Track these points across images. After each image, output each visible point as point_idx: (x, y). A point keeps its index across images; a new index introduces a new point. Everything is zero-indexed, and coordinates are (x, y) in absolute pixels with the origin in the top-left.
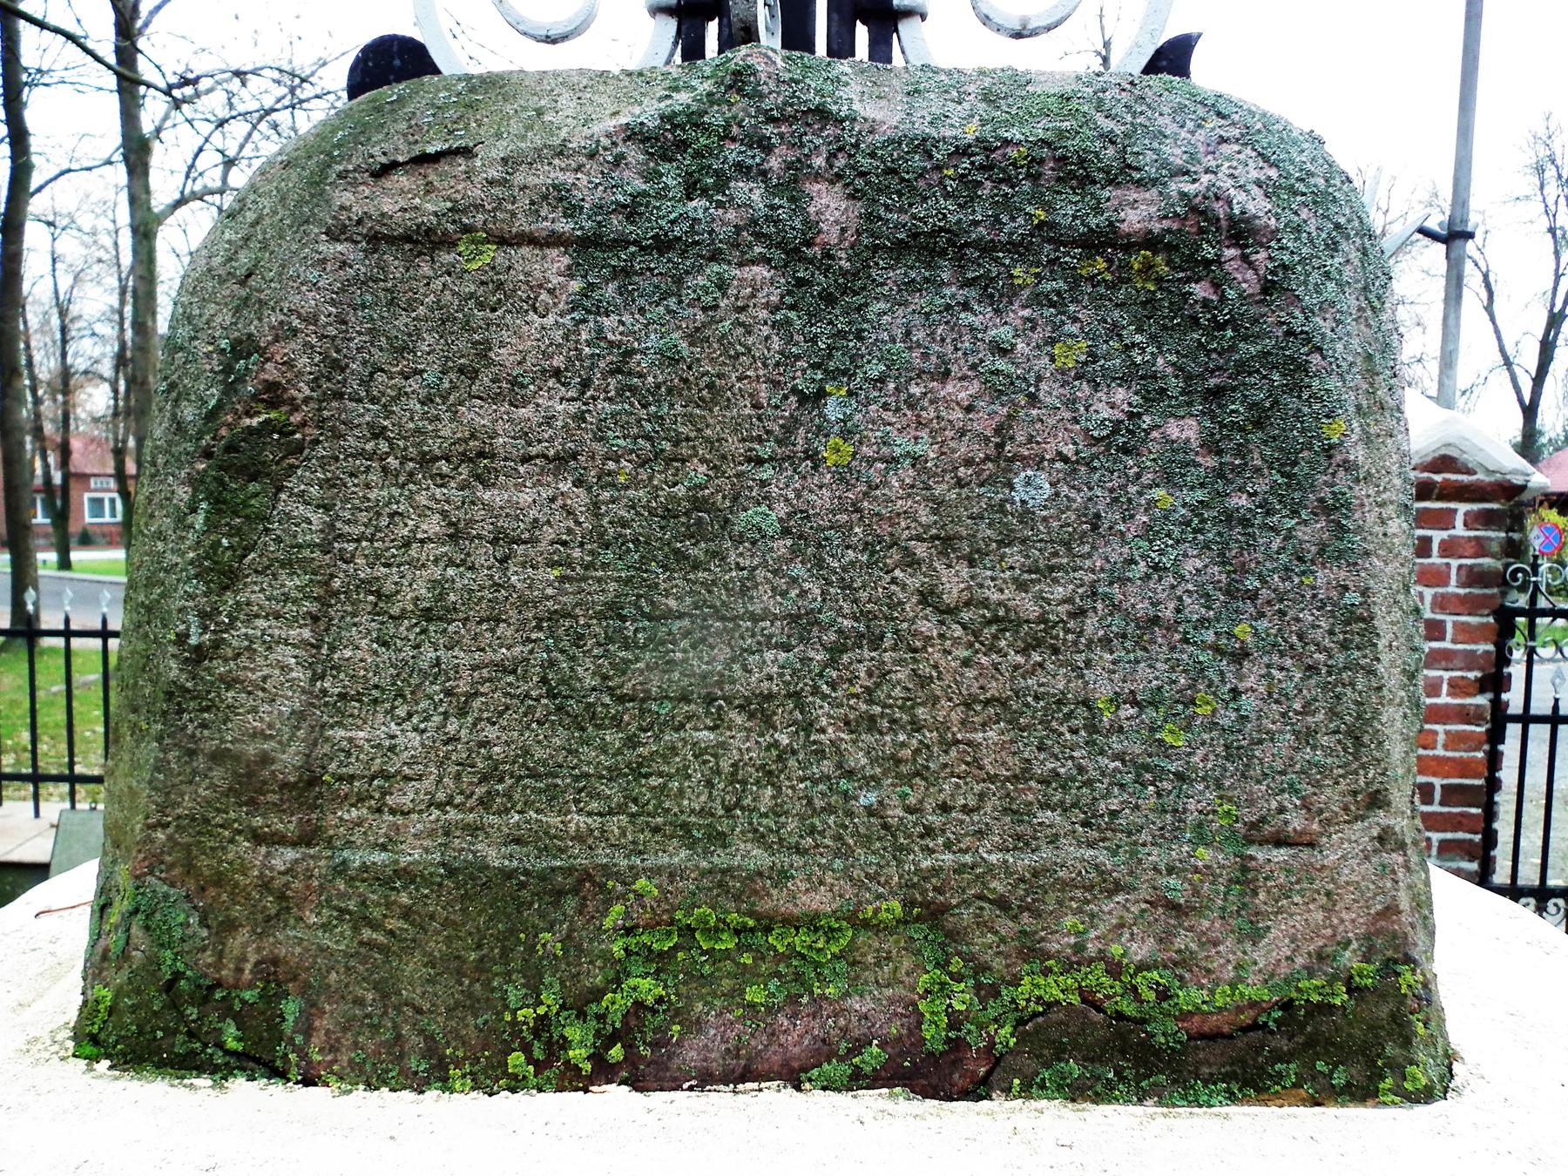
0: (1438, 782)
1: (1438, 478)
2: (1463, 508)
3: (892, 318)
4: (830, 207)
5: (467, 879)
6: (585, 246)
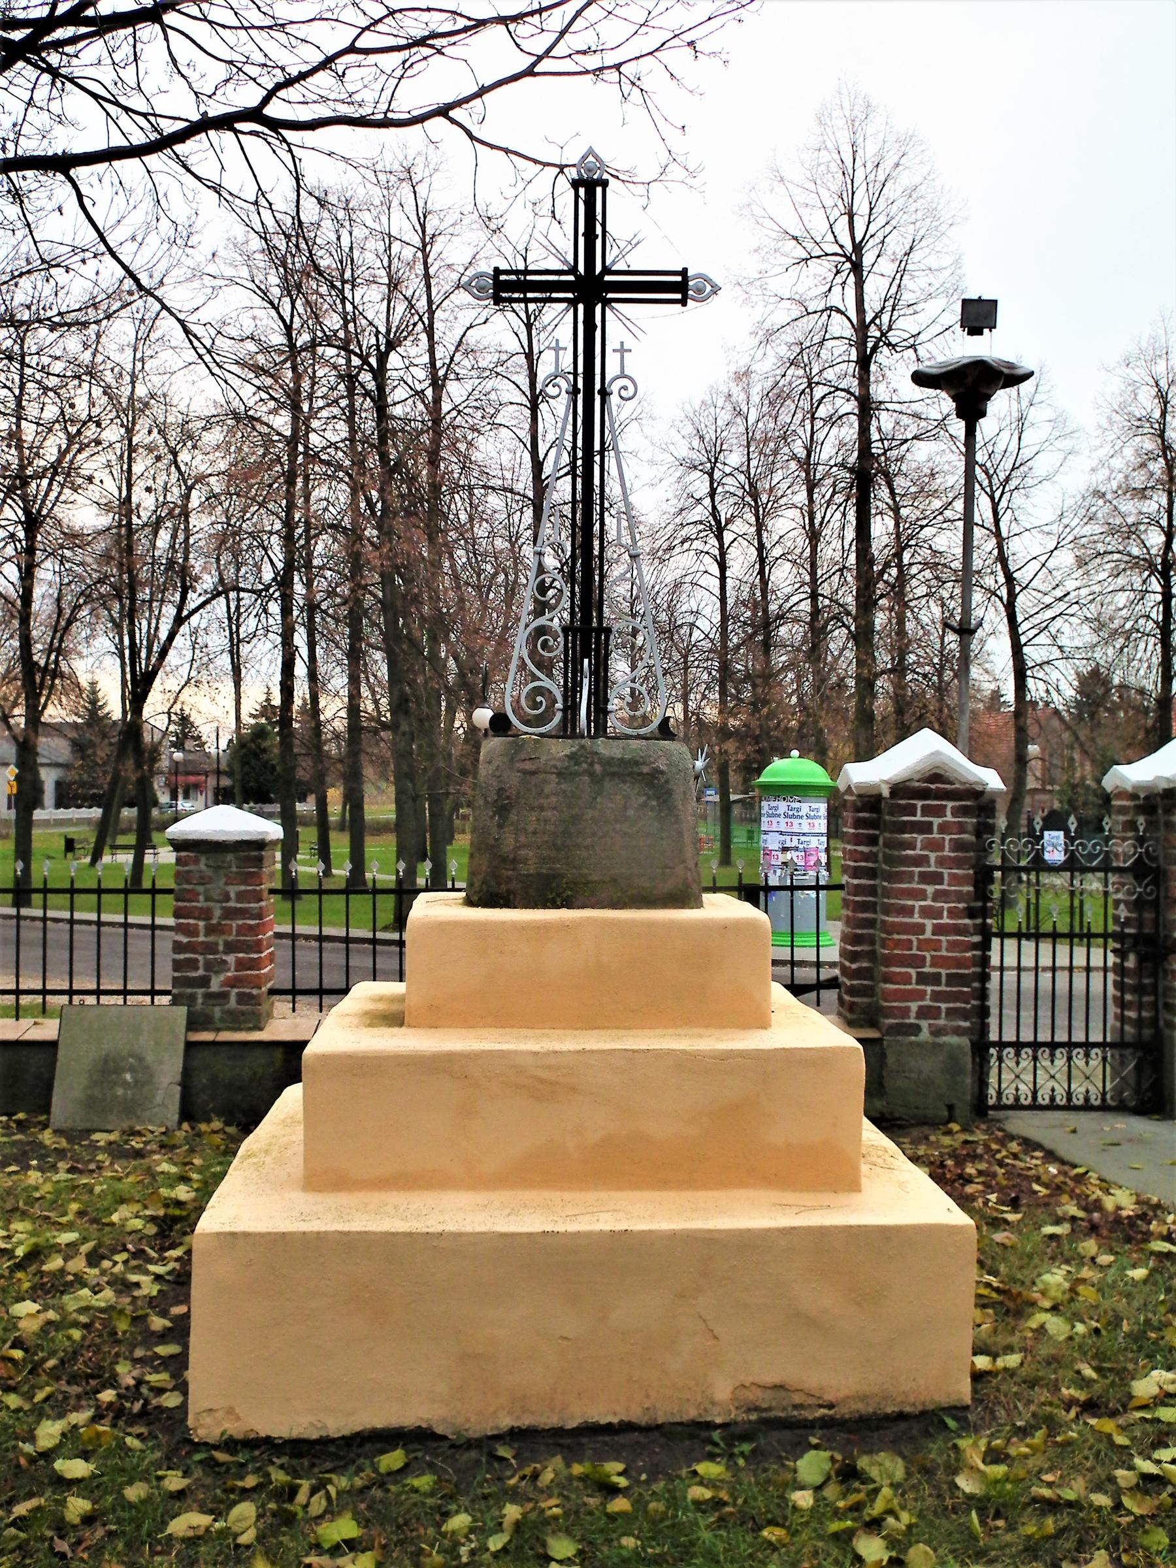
0: (943, 972)
1: (933, 786)
2: (950, 804)
3: (608, 785)
4: (598, 768)
5: (539, 875)
6: (559, 774)
